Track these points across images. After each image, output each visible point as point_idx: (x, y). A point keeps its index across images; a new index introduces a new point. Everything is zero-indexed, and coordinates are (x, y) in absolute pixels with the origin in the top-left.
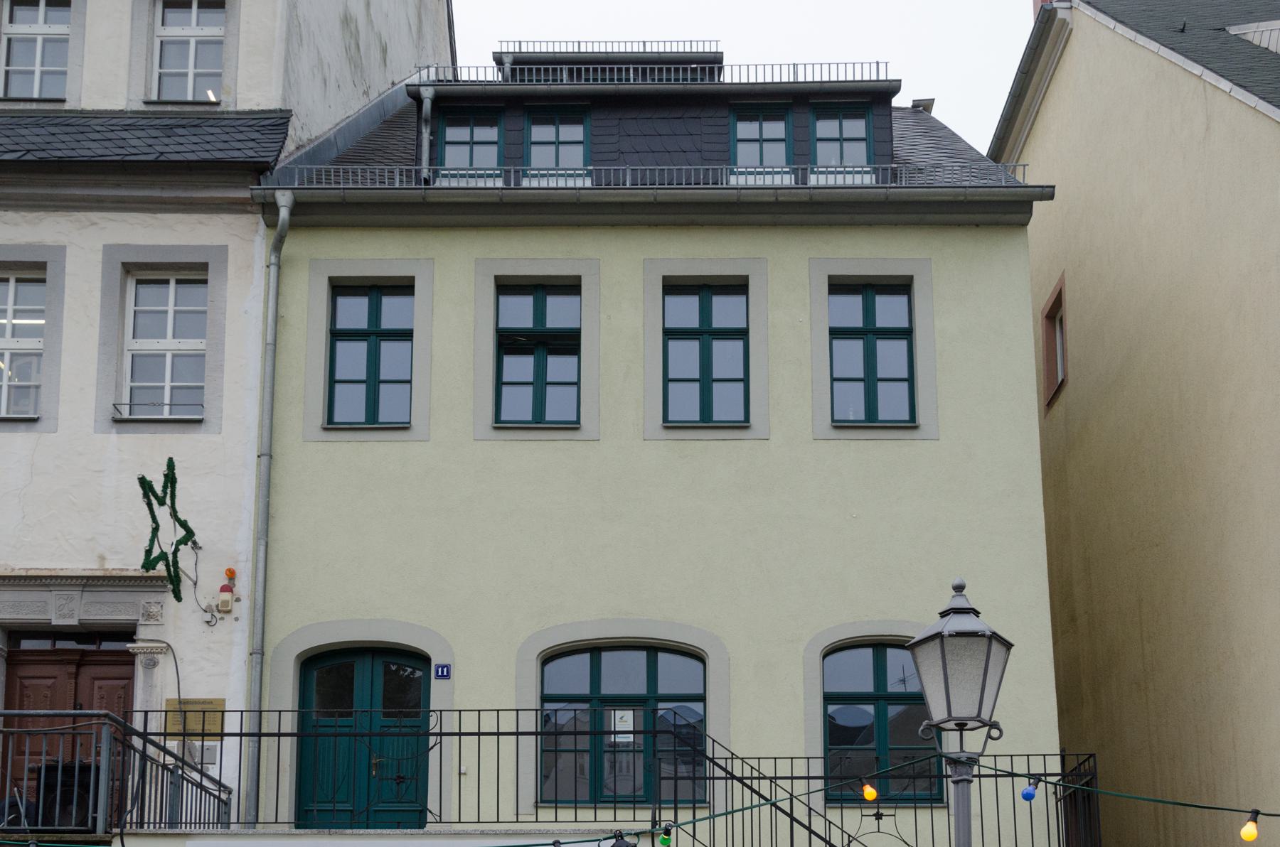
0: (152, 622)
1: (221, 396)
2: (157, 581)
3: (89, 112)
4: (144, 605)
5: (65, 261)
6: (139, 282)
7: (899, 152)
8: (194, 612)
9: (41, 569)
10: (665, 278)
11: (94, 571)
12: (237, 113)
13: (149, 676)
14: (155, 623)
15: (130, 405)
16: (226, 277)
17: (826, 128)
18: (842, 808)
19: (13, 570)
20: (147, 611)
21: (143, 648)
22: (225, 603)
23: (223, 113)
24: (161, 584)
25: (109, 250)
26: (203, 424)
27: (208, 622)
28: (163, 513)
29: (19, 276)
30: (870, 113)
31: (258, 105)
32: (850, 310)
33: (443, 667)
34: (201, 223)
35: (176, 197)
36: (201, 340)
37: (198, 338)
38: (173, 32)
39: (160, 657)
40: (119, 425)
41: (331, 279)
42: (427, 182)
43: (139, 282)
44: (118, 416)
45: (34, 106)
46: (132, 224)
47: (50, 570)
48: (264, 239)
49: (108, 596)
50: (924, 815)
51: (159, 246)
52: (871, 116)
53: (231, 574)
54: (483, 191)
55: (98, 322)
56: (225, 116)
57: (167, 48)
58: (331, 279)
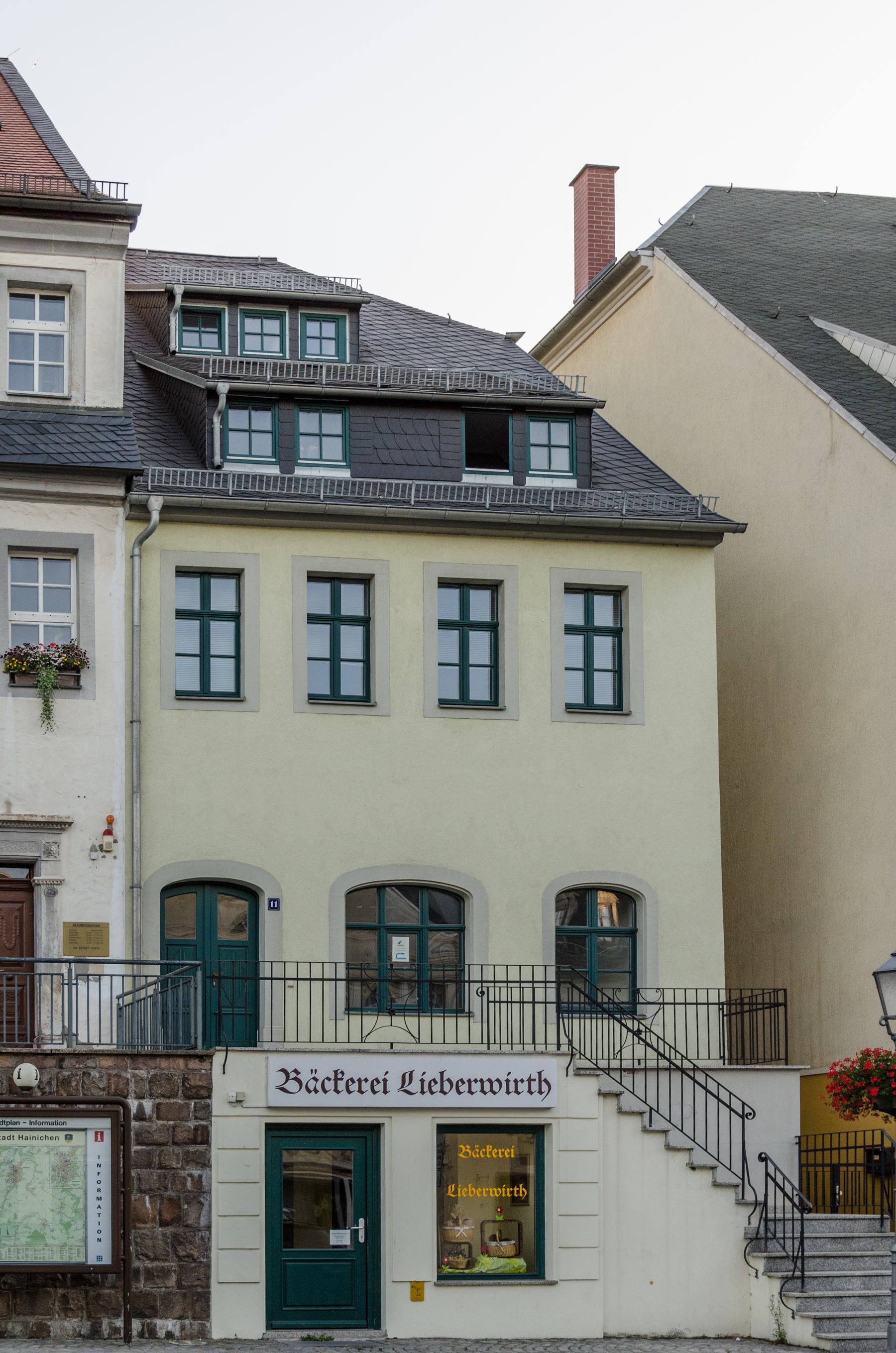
0: (51, 858)
13: (50, 903)
14: (55, 859)
17: (307, 421)
18: (404, 1016)
22: (109, 844)
23: (74, 407)
26: (81, 691)
30: (276, 407)
31: (104, 403)
33: (274, 900)
35: (702, 539)
50: (450, 1022)
52: (277, 410)
53: (110, 821)
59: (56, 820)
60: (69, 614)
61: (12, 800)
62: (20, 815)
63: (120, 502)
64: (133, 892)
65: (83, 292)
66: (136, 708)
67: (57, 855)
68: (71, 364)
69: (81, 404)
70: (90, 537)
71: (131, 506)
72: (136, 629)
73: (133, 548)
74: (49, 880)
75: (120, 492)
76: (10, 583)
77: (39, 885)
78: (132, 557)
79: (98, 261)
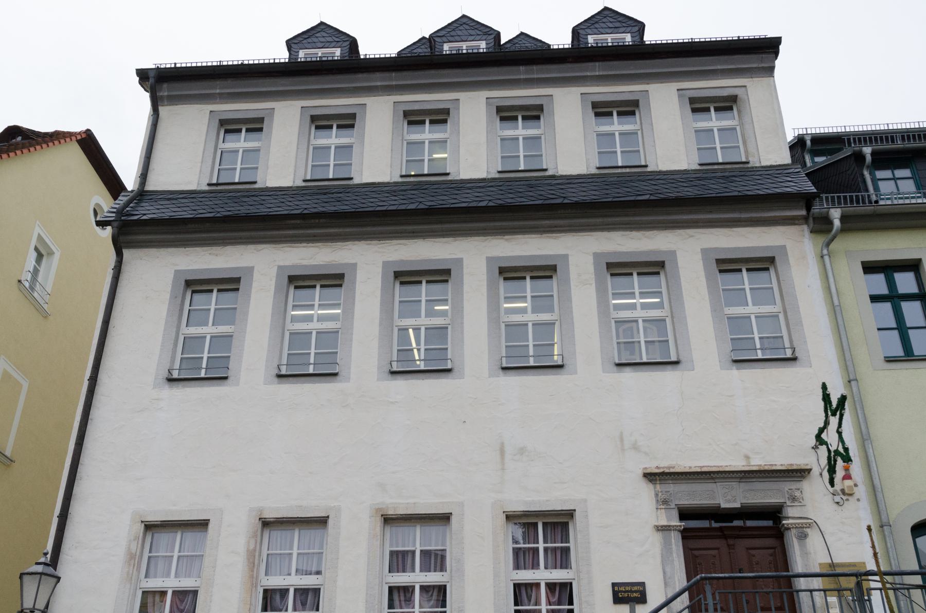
0: (796, 504)
1: (805, 342)
2: (796, 473)
3: (664, 172)
4: (787, 491)
5: (677, 260)
6: (296, 287)
8: (825, 495)
9: (711, 467)
11: (751, 467)
13: (803, 547)
15: (206, 369)
16: (789, 264)
19: (690, 467)
20: (792, 496)
21: (795, 524)
22: (849, 487)
23: (753, 168)
24: (800, 475)
25: (386, 264)
27: (838, 503)
28: (834, 421)
29: (428, 279)
31: (776, 162)
32: (878, 283)
36: (231, 326)
37: (442, 317)
38: (229, 145)
39: (808, 530)
40: (619, 367)
41: (863, 263)
42: (876, 202)
43: (193, 292)
44: (170, 377)
45: (619, 171)
46: (717, 236)
48: (810, 240)
49: (758, 485)
51: (739, 248)
54: (909, 205)
55: (708, 297)
56: (755, 169)
57: (224, 154)
58: (863, 263)
59: (795, 467)
60: (775, 306)
61: (751, 455)
62: (761, 465)
63: (803, 221)
64: (883, 531)
65: (746, 98)
66: (851, 369)
67: (801, 500)
68: (745, 142)
69: (758, 165)
70: (784, 247)
71: (814, 219)
72: (837, 309)
73: (822, 250)
74: (798, 524)
75: (804, 213)
76: (721, 288)
77: (789, 529)
78: (822, 257)
79: (754, 79)
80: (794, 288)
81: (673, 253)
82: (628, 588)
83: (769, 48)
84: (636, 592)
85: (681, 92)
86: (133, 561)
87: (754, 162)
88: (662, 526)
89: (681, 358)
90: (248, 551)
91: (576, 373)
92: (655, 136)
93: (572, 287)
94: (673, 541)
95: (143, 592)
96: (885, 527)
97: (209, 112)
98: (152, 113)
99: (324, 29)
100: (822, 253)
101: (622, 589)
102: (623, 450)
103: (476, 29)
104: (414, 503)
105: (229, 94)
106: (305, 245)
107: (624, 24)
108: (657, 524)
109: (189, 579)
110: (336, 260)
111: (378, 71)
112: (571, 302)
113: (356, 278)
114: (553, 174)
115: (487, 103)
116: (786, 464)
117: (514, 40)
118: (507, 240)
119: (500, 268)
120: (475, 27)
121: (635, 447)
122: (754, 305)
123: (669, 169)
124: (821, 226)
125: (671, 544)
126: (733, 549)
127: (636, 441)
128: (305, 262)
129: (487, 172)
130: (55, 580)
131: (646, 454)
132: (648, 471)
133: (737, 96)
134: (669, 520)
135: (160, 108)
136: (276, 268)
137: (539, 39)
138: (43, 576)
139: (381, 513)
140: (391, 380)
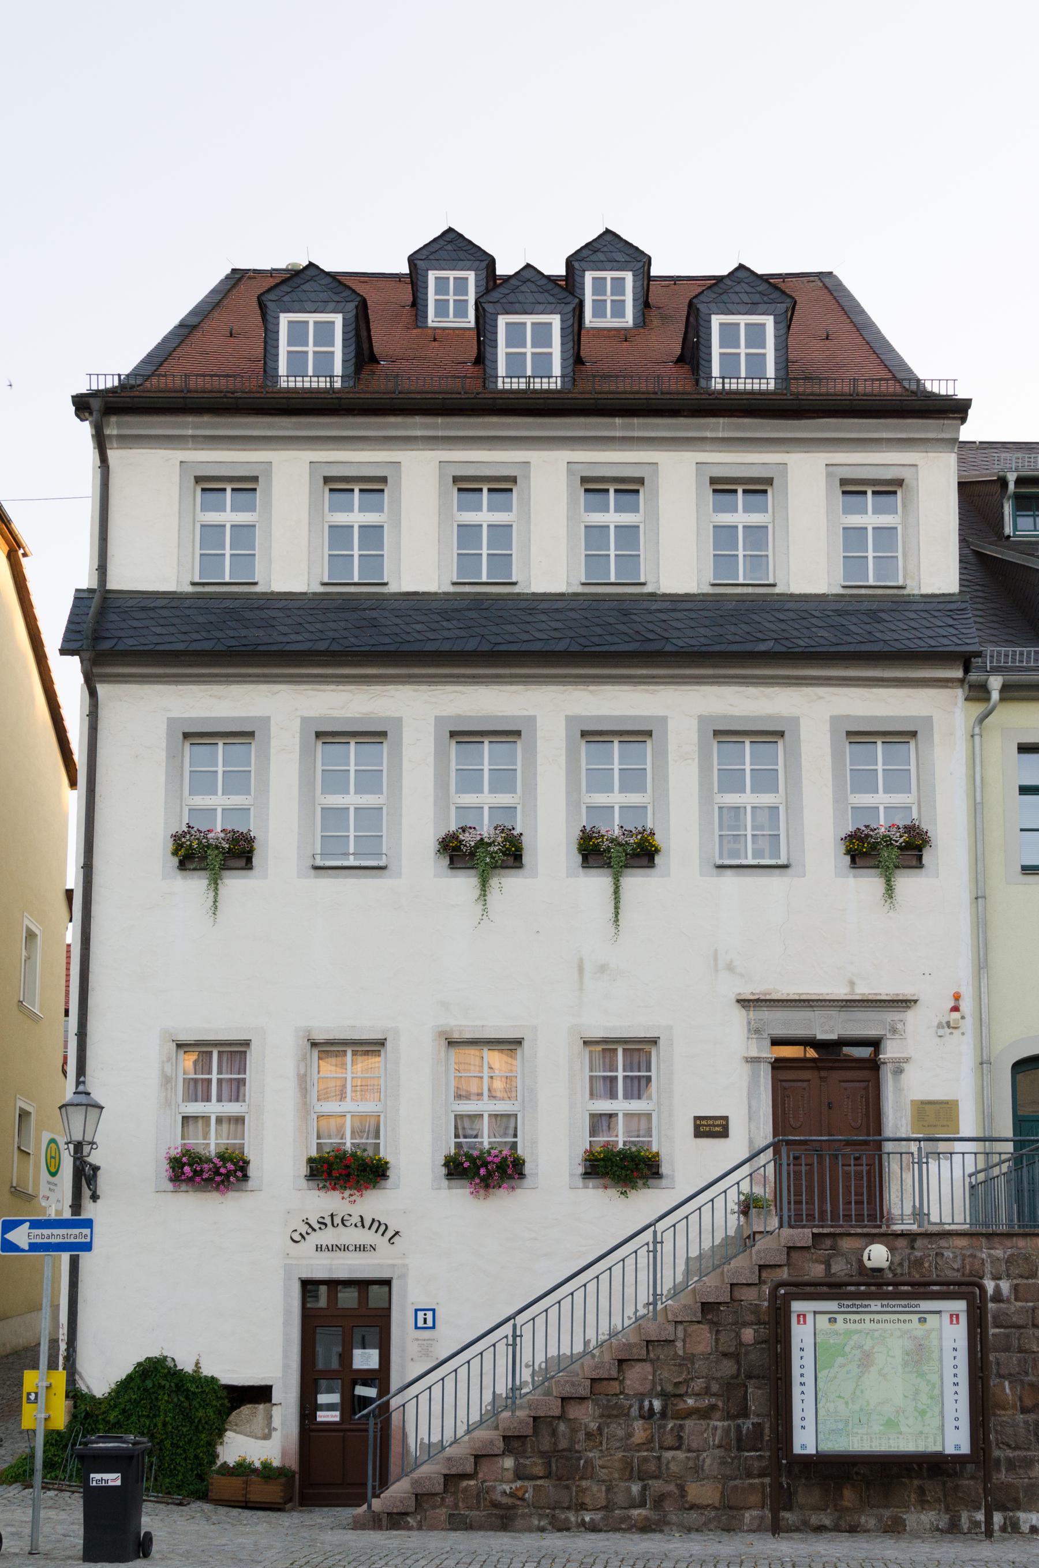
7: (1006, 638)
10: (1018, 744)
12: (922, 596)
13: (897, 1081)
19: (788, 994)
25: (835, 720)
34: (909, 697)
37: (510, 793)
40: (720, 869)
47: (819, 995)
53: (957, 997)
59: (901, 998)
64: (982, 1068)
68: (905, 555)
69: (916, 592)
70: (929, 718)
72: (978, 807)
73: (974, 728)
74: (896, 1058)
75: (959, 674)
78: (972, 736)
80: (934, 775)
81: (795, 721)
82: (710, 1122)
83: (953, 412)
84: (718, 1126)
85: (831, 468)
86: (169, 1085)
87: (913, 589)
88: (751, 1058)
89: (792, 861)
90: (298, 1075)
91: (668, 875)
92: (790, 539)
93: (671, 763)
94: (762, 1073)
95: (183, 1117)
96: (985, 1065)
97: (178, 464)
98: (99, 465)
99: (316, 276)
100: (973, 731)
101: (704, 1122)
102: (716, 970)
103: (546, 291)
104: (483, 1026)
105: (205, 437)
106: (333, 687)
107: (765, 298)
108: (746, 1055)
109: (236, 1103)
110: (376, 711)
111: (417, 414)
112: (668, 783)
113: (401, 738)
114: (653, 591)
115: (568, 470)
116: (891, 993)
117: (594, 244)
118: (591, 692)
119: (582, 731)
120: (544, 287)
121: (730, 968)
122: (885, 792)
123: (803, 591)
124: (978, 692)
125: (759, 1077)
126: (824, 1082)
127: (731, 961)
128: (336, 713)
129: (567, 583)
130: (97, 1110)
131: (742, 975)
132: (742, 997)
133: (903, 480)
134: (760, 1051)
135: (110, 453)
136: (299, 720)
137: (635, 244)
138: (89, 1108)
139: (445, 1037)
140: (451, 877)
